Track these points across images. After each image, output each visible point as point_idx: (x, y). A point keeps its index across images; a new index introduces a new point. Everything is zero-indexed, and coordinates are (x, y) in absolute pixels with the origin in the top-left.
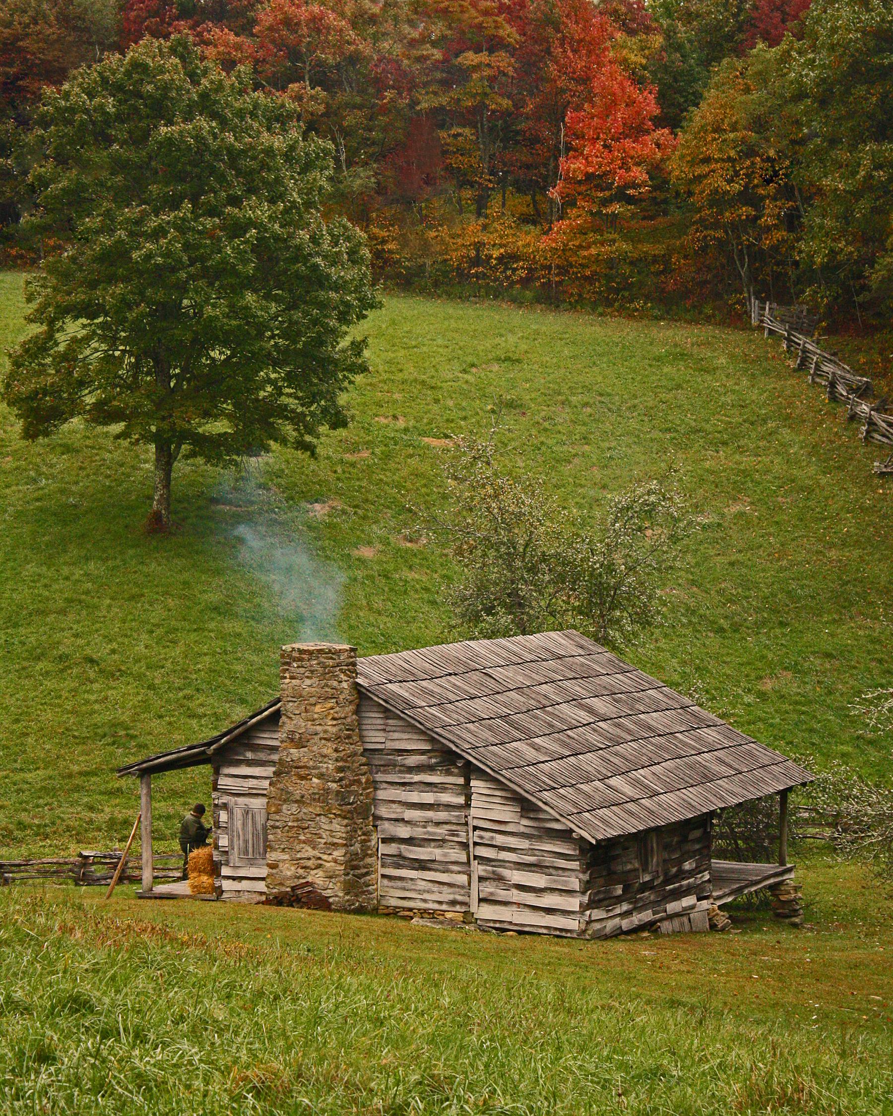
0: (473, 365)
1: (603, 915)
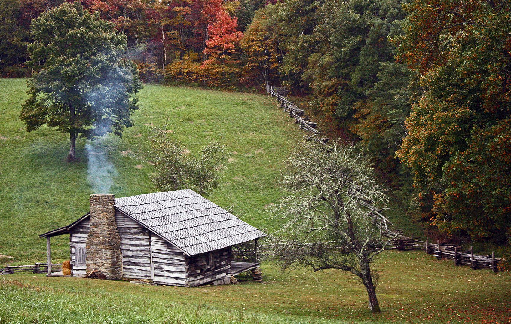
0: (176, 107)
1: (194, 279)
